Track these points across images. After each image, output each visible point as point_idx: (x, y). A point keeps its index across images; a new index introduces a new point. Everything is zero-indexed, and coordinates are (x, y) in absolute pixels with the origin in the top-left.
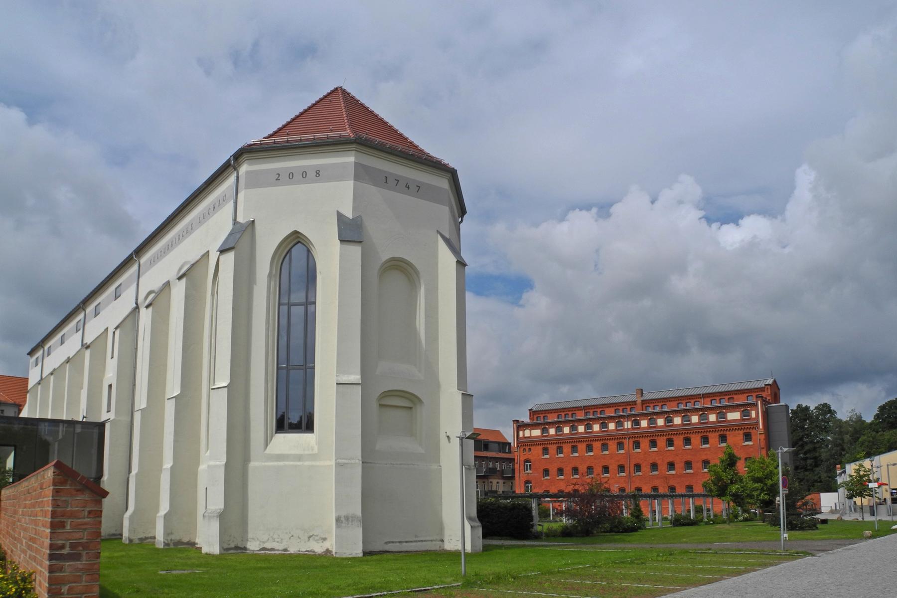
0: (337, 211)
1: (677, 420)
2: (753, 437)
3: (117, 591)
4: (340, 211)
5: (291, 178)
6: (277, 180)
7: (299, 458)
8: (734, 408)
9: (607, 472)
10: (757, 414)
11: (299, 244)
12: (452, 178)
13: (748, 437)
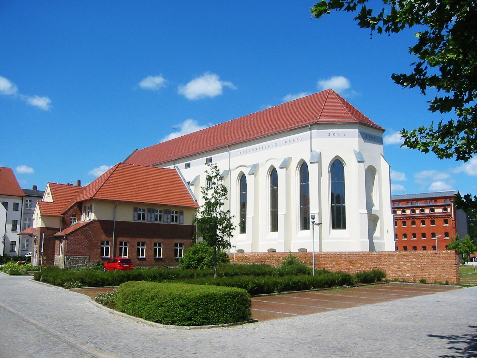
0: (428, 110)
1: (408, 212)
2: (449, 222)
3: (78, 209)
4: (428, 109)
6: (329, 135)
8: (438, 206)
9: (415, 237)
10: (451, 210)
13: (446, 222)
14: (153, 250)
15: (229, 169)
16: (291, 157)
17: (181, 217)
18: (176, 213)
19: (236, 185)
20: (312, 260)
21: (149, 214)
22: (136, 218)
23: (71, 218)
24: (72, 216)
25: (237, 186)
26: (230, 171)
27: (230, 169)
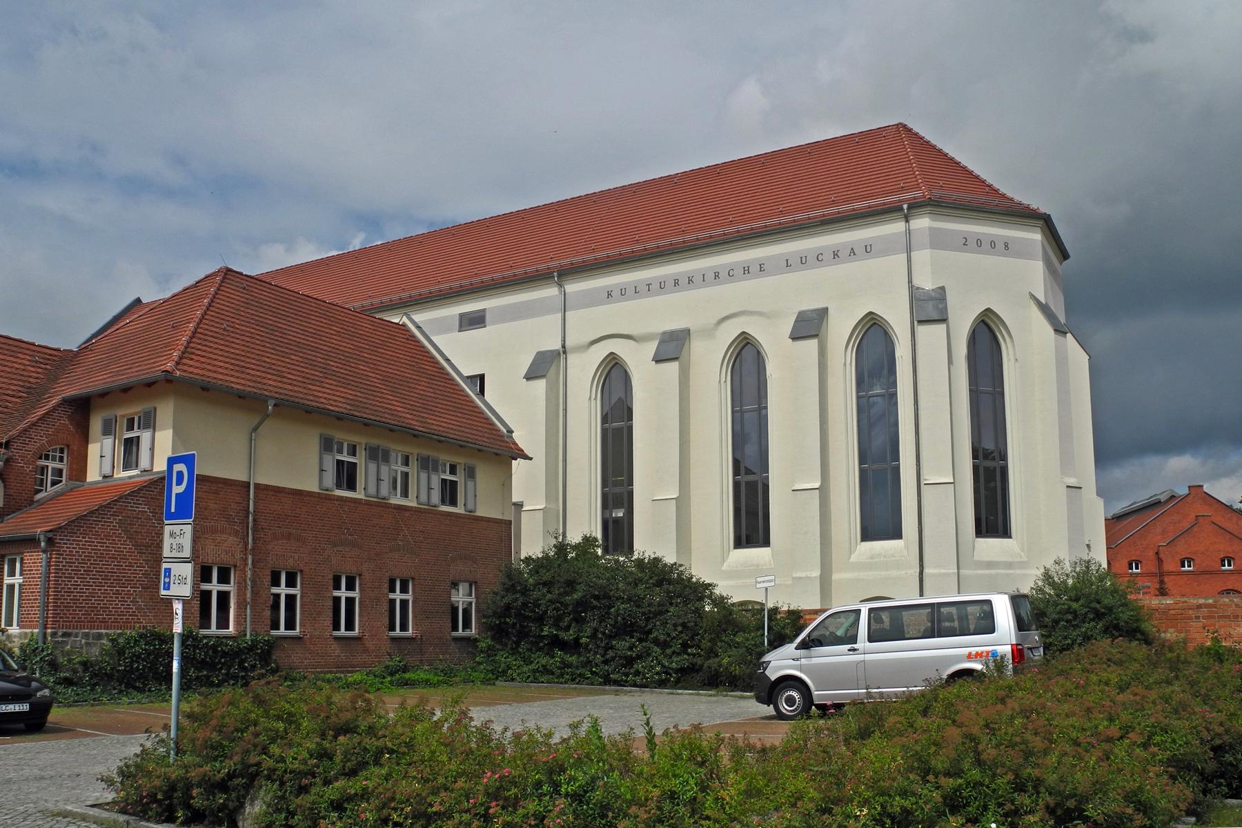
5: (804, 262)
7: (1009, 565)
11: (876, 326)
12: (1045, 225)
14: (386, 607)
15: (558, 346)
16: (827, 309)
17: (470, 484)
18: (453, 470)
19: (590, 399)
20: (26, 633)
21: (372, 467)
22: (330, 479)
23: (43, 463)
24: (47, 457)
25: (593, 402)
26: (565, 352)
27: (564, 347)
